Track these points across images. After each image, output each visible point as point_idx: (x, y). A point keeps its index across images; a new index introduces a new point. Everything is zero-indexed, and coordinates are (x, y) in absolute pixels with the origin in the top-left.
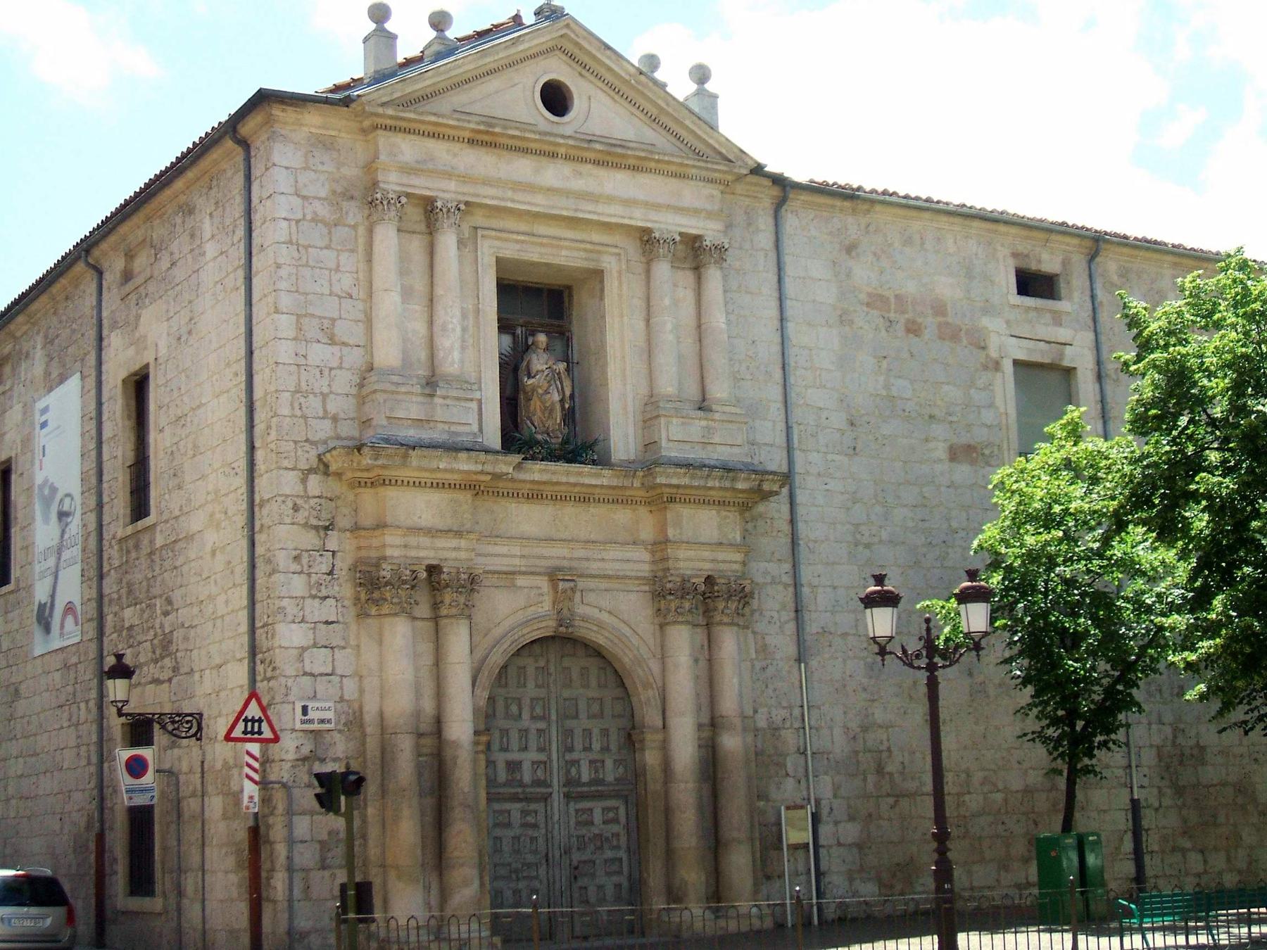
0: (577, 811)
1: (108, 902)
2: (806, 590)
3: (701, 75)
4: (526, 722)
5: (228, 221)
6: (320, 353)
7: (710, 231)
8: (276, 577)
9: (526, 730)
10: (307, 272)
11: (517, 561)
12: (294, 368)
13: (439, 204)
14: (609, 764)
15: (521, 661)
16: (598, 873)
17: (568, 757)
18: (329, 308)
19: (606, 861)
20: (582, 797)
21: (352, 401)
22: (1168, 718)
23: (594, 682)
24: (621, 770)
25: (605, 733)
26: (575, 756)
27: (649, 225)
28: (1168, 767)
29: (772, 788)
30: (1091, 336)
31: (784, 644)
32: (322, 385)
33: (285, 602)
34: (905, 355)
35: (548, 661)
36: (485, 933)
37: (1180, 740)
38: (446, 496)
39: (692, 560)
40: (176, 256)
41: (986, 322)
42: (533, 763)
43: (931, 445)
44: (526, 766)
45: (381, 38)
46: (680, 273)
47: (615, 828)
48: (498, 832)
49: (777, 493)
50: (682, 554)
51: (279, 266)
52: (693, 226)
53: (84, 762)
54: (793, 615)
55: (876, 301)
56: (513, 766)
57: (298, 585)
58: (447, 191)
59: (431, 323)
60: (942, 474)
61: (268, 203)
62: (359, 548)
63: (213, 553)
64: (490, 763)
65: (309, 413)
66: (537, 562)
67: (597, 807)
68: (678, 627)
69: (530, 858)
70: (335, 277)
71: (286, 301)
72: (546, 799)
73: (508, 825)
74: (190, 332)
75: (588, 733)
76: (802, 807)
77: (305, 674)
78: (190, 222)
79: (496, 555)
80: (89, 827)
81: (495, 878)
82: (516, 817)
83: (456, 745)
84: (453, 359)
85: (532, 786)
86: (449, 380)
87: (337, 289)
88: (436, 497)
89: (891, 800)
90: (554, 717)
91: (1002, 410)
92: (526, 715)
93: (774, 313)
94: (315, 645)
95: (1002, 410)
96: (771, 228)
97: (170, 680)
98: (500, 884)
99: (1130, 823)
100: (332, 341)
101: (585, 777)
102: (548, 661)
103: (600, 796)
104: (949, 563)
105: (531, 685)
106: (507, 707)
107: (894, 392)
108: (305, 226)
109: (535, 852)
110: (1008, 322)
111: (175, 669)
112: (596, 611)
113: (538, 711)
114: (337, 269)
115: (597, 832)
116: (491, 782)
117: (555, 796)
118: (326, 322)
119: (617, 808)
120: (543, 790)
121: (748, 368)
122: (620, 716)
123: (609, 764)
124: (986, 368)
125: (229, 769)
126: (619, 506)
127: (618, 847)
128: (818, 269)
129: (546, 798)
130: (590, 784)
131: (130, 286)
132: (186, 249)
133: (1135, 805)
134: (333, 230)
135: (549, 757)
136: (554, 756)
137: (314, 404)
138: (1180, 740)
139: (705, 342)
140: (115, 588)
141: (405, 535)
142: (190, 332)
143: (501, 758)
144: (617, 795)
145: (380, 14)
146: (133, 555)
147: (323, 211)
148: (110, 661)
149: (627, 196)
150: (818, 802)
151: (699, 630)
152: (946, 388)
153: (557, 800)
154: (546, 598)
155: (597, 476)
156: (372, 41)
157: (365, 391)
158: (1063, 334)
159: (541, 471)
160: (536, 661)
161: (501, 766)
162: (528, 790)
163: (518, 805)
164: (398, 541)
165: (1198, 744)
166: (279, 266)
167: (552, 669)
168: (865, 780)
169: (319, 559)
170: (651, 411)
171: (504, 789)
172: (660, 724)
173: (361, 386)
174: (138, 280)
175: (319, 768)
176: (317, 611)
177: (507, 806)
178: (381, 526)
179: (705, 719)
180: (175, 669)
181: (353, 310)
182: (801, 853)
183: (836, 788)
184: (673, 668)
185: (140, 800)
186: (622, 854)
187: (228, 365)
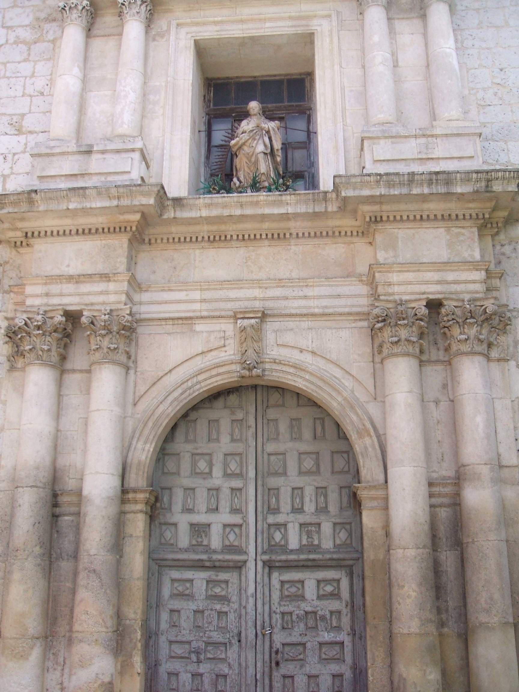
0: (282, 583)
4: (217, 478)
9: (217, 489)
11: (197, 306)
14: (327, 528)
16: (309, 659)
17: (271, 519)
19: (321, 644)
20: (288, 566)
23: (307, 434)
24: (343, 535)
25: (321, 491)
26: (280, 518)
38: (99, 242)
39: (410, 283)
42: (225, 526)
44: (216, 532)
47: (335, 605)
50: (395, 277)
56: (199, 530)
66: (222, 305)
67: (310, 580)
68: (395, 360)
69: (217, 637)
70: (29, 81)
72: (240, 568)
79: (166, 302)
85: (222, 552)
88: (89, 245)
92: (217, 472)
101: (293, 543)
103: (314, 565)
105: (225, 439)
106: (194, 464)
109: (223, 630)
112: (296, 353)
113: (233, 466)
115: (309, 609)
117: (251, 565)
119: (338, 581)
121: (496, 94)
122: (341, 472)
123: (327, 528)
126: (328, 241)
127: (338, 628)
129: (239, 567)
130: (301, 550)
134: (32, 47)
141: (46, 284)
147: (25, 34)
154: (231, 341)
155: (280, 203)
159: (208, 206)
160: (233, 413)
164: (39, 289)
172: (381, 478)
177: (189, 574)
184: (396, 412)
186: (344, 637)
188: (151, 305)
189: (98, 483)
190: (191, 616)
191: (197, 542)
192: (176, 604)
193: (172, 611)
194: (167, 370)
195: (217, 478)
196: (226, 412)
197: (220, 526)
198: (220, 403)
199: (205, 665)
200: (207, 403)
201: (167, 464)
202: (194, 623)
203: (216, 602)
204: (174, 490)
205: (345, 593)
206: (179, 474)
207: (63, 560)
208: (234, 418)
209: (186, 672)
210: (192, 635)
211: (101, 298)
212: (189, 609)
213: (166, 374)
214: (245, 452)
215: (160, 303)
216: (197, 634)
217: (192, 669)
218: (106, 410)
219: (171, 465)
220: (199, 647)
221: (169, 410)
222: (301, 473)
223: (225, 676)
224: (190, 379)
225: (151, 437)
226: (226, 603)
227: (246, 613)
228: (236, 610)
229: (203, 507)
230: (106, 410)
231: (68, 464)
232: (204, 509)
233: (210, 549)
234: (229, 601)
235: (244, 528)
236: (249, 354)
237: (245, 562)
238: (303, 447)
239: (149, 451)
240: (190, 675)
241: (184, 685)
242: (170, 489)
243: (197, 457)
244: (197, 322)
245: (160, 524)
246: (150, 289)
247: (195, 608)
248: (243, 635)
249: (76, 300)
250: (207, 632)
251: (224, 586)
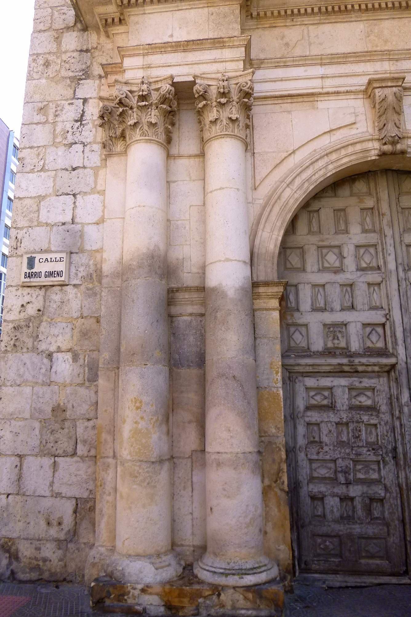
35: (378, 200)
44: (354, 330)
73: (331, 407)
77: (40, 224)
82: (342, 399)
90: (392, 265)
92: (350, 263)
102: (378, 200)
105: (355, 229)
120: (384, 361)
135: (387, 316)
160: (361, 201)
162: (357, 361)
163: (343, 382)
167: (385, 207)
169: (67, 107)
176: (59, 157)
177: (326, 382)
188: (267, 82)
189: (227, 274)
190: (333, 429)
191: (334, 344)
192: (314, 416)
193: (309, 424)
194: (291, 149)
196: (353, 201)
197: (359, 326)
198: (345, 191)
199: (356, 487)
200: (330, 192)
201: (289, 259)
202: (337, 437)
203: (362, 412)
204: (301, 287)
206: (304, 270)
207: (183, 367)
208: (363, 206)
209: (334, 495)
210: (337, 452)
211: (213, 68)
212: (331, 422)
213: (290, 154)
214: (380, 242)
215: (275, 81)
216: (343, 451)
217: (340, 492)
218: (231, 188)
219: (294, 260)
220: (347, 467)
221: (293, 196)
223: (381, 501)
224: (296, 177)
225: (279, 224)
226: (374, 413)
227: (401, 425)
228: (387, 422)
230: (231, 188)
231: (181, 257)
232: (338, 308)
233: (350, 351)
234: (378, 411)
235: (387, 327)
236: (389, 128)
239: (277, 240)
240: (337, 499)
241: (332, 511)
242: (296, 286)
243: (325, 251)
244: (319, 99)
245: (288, 325)
246: (262, 66)
247: (337, 420)
248: (400, 449)
249: (185, 70)
250: (355, 449)
251: (369, 394)
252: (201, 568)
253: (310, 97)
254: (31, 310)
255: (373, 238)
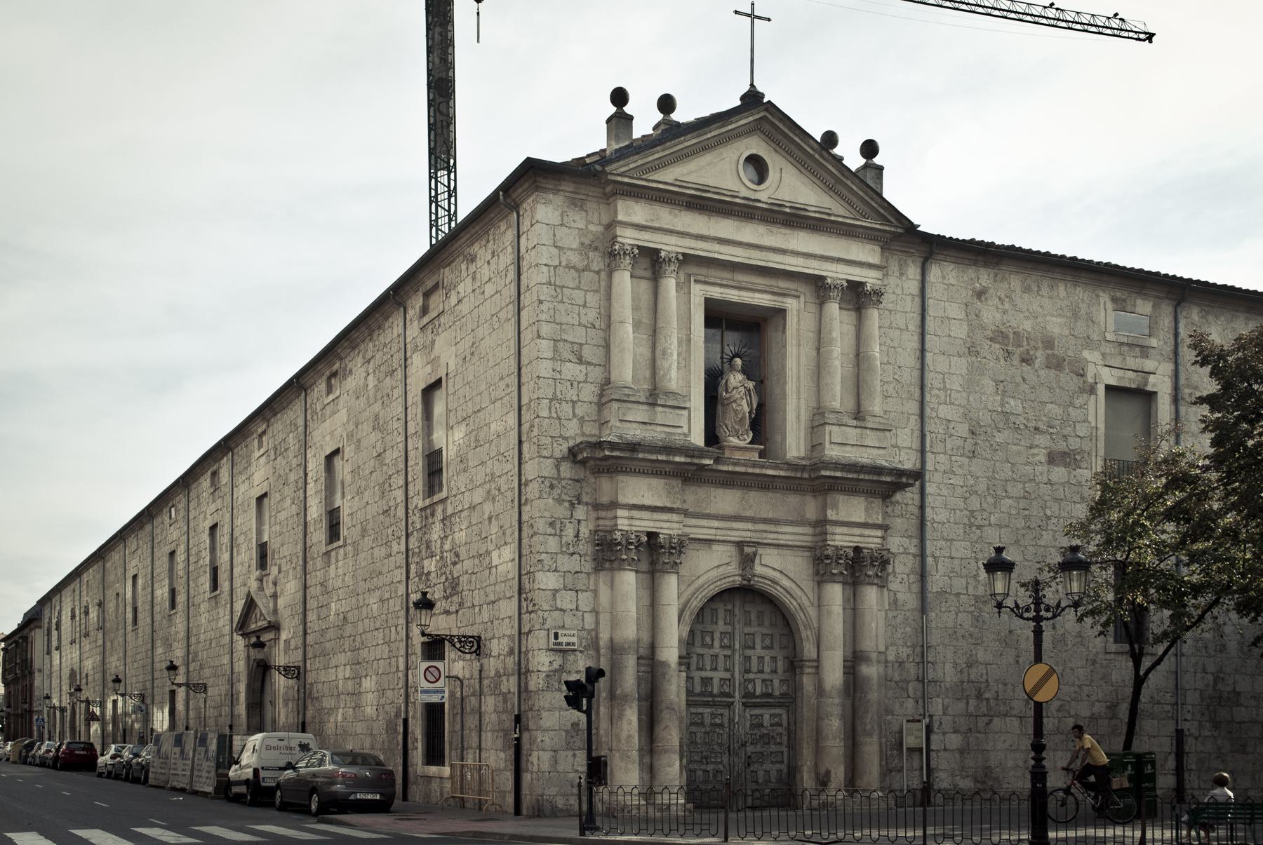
1: (410, 769)
2: (930, 560)
3: (869, 149)
4: (717, 649)
5: (502, 267)
6: (572, 370)
7: (870, 278)
8: (536, 538)
9: (717, 656)
10: (560, 307)
12: (551, 381)
13: (663, 254)
14: (776, 683)
15: (714, 606)
18: (578, 335)
20: (755, 706)
21: (595, 407)
22: (1211, 668)
23: (767, 623)
24: (785, 687)
25: (774, 659)
26: (751, 676)
27: (824, 274)
28: (1208, 706)
29: (897, 706)
30: (1171, 366)
31: (909, 599)
32: (572, 394)
33: (543, 556)
34: (1019, 379)
36: (682, 801)
37: (1220, 686)
40: (462, 295)
41: (1086, 354)
43: (1035, 451)
44: (716, 682)
45: (620, 121)
46: (844, 312)
47: (780, 729)
48: (694, 729)
49: (911, 485)
51: (541, 302)
52: (857, 274)
53: (394, 669)
54: (918, 577)
55: (999, 336)
57: (553, 544)
58: (669, 246)
59: (654, 348)
60: (1042, 474)
61: (533, 252)
62: (598, 519)
63: (490, 518)
64: (689, 678)
65: (562, 415)
67: (766, 714)
70: (583, 311)
71: (546, 329)
73: (702, 724)
74: (472, 354)
75: (761, 659)
76: (919, 721)
77: (557, 609)
78: (472, 268)
80: (397, 715)
81: (690, 762)
82: (707, 720)
83: (665, 664)
84: (673, 379)
86: (669, 393)
87: (584, 321)
89: (986, 719)
90: (737, 646)
91: (1093, 424)
92: (717, 644)
93: (915, 344)
94: (565, 589)
95: (1093, 424)
96: (919, 277)
97: (457, 612)
98: (695, 766)
99: (1174, 748)
100: (580, 361)
104: (1042, 543)
105: (721, 622)
106: (703, 638)
107: (1008, 409)
108: (560, 271)
110: (1103, 355)
111: (461, 604)
114: (585, 306)
116: (690, 692)
118: (576, 347)
123: (776, 683)
124: (1082, 391)
125: (500, 676)
127: (780, 744)
128: (955, 311)
131: (426, 320)
132: (469, 290)
133: (1180, 736)
135: (733, 676)
136: (737, 675)
137: (567, 408)
138: (1220, 686)
139: (861, 368)
140: (417, 544)
142: (472, 354)
143: (697, 675)
144: (780, 705)
145: (619, 97)
146: (430, 520)
147: (575, 258)
148: (415, 597)
149: (802, 250)
150: (931, 716)
151: (847, 587)
152: (1050, 406)
153: (738, 707)
156: (614, 121)
157: (604, 400)
158: (1149, 365)
161: (697, 681)
163: (708, 710)
165: (1234, 691)
166: (541, 302)
167: (737, 612)
168: (968, 703)
170: (818, 421)
171: (698, 697)
173: (601, 396)
174: (433, 314)
175: (565, 677)
176: (566, 563)
177: (701, 710)
178: (614, 505)
179: (849, 654)
180: (461, 604)
181: (596, 336)
182: (916, 756)
183: (945, 708)
185: (435, 699)
186: (785, 750)
187: (502, 379)
195: (717, 649)
205: (785, 723)
222: (763, 648)
229: (708, 668)
237: (732, 703)
238: (765, 631)
252: (1077, 809)
253: (709, 542)
254: (556, 666)
255: (729, 629)
